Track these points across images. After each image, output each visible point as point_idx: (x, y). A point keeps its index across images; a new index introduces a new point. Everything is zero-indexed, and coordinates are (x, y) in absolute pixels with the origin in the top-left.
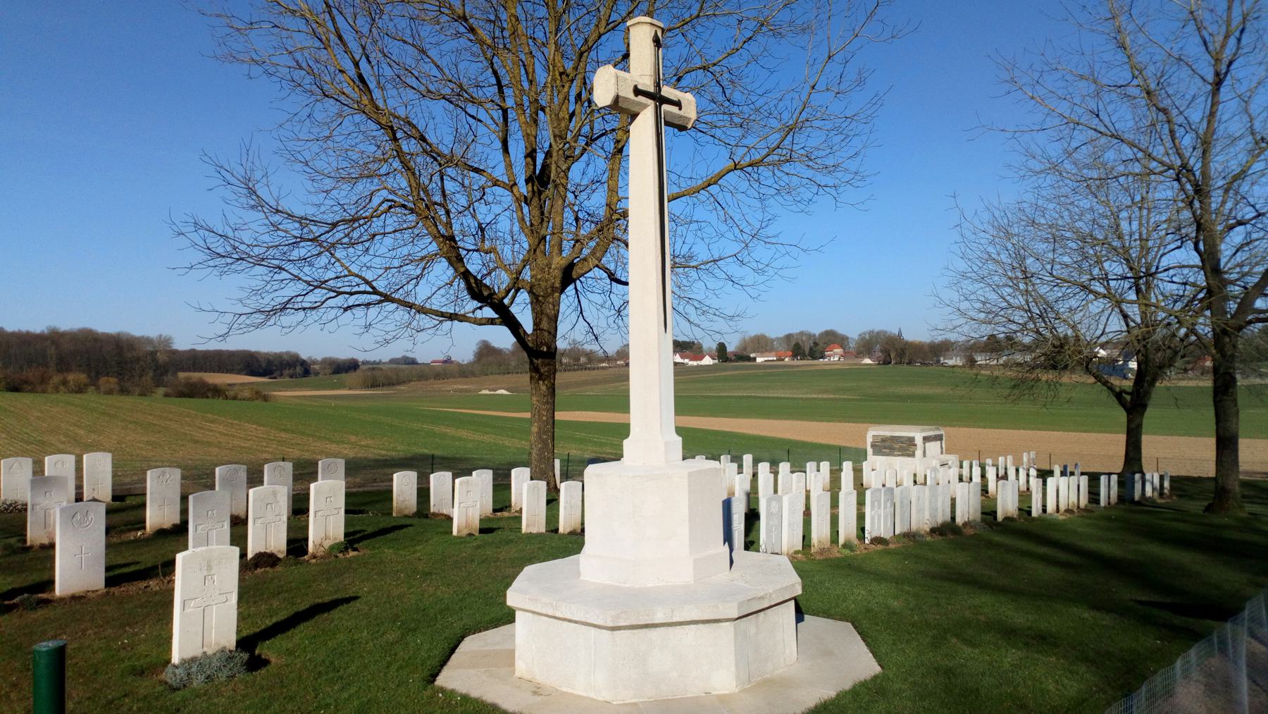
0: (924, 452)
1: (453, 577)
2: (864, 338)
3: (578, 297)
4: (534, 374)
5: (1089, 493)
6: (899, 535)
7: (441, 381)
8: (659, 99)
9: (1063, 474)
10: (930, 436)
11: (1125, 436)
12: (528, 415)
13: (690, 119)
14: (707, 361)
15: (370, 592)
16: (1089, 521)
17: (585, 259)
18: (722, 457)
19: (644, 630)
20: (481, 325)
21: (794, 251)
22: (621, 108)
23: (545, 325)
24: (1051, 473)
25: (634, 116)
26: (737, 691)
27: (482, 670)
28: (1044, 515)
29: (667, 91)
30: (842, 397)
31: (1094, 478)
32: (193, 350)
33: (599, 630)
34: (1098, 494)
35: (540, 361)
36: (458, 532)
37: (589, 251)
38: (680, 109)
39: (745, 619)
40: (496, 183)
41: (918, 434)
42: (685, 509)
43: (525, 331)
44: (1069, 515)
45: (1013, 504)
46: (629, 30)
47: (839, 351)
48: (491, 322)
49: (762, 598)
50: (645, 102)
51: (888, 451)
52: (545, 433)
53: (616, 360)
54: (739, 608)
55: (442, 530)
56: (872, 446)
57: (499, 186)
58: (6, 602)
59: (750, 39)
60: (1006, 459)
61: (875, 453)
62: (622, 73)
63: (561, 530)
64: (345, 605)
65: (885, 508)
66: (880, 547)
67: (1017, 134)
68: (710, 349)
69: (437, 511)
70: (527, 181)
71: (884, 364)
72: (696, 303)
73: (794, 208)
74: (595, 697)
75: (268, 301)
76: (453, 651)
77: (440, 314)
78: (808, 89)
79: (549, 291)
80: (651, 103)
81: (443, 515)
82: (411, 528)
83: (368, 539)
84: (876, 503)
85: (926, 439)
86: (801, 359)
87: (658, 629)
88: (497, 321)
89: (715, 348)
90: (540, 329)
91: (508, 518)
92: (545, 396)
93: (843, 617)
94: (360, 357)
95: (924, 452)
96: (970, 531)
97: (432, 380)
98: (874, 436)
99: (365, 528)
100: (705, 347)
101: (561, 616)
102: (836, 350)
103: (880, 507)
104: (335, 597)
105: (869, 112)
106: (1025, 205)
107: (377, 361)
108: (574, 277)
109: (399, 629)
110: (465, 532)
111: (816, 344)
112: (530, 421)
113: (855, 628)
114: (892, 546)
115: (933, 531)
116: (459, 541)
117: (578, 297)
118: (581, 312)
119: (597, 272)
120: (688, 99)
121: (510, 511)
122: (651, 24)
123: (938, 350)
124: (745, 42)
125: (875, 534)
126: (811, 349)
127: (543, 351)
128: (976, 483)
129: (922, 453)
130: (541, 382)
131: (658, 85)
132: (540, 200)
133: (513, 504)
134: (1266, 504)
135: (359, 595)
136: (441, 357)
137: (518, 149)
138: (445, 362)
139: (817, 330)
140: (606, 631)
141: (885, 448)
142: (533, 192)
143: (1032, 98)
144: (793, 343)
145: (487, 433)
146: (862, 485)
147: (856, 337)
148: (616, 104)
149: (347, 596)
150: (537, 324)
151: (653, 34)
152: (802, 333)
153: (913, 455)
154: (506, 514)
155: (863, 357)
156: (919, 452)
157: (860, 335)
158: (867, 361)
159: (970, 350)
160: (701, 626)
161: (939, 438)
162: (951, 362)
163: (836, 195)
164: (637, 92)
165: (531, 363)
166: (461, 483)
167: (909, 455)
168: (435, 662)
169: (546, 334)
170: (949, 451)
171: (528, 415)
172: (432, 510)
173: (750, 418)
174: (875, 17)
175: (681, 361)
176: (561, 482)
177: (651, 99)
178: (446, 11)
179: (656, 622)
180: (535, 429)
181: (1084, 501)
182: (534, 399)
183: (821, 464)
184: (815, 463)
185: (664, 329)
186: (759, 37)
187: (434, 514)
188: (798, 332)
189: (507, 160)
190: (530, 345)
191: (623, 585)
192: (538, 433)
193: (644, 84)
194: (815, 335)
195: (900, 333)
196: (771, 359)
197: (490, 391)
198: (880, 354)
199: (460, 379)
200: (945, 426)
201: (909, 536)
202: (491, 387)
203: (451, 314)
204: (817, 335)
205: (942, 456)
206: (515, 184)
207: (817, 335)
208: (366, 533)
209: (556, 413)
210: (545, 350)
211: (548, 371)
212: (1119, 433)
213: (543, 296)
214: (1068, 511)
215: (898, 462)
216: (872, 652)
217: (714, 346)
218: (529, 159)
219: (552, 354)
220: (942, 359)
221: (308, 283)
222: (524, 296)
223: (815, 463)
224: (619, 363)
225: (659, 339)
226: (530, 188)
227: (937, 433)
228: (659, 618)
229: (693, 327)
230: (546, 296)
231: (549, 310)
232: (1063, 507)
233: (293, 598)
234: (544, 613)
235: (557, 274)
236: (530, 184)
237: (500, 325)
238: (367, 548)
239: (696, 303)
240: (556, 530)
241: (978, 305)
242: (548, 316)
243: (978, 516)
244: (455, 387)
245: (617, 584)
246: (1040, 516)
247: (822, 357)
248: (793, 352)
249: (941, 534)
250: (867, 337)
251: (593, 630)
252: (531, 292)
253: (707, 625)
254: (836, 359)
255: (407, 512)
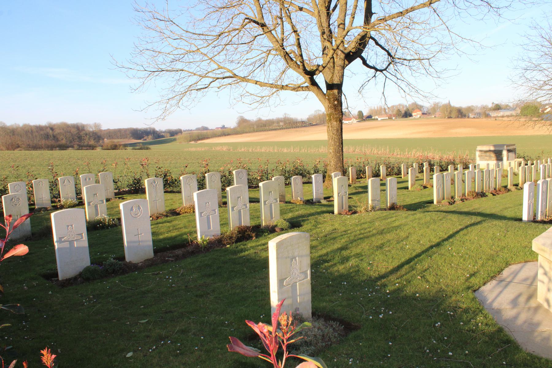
32: (109, 129)
51: (488, 158)
58: (2, 252)
75: (180, 89)
89: (357, 114)
94: (183, 128)
107: (190, 129)
136: (220, 126)
152: (400, 105)
176: (334, 178)
196: (386, 118)
221: (200, 76)
233: (221, 256)
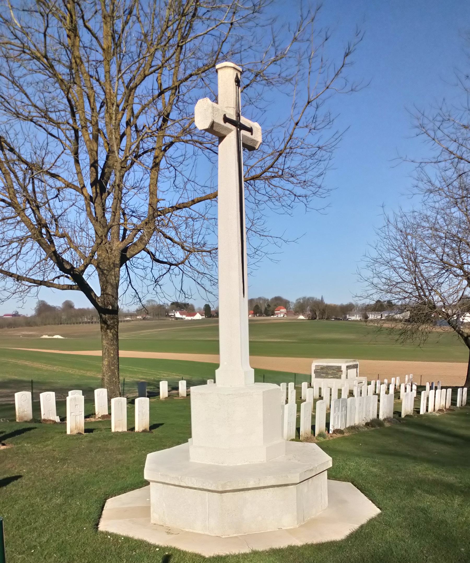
0: (347, 376)
1: (82, 461)
2: (300, 302)
3: (128, 271)
4: (103, 325)
5: (452, 400)
6: (349, 427)
7: (13, 329)
8: (240, 127)
9: (431, 388)
10: (350, 366)
11: (468, 364)
12: (99, 353)
13: (257, 142)
14: (198, 317)
15: (28, 473)
16: (455, 417)
17: (135, 244)
18: (208, 381)
19: (241, 492)
20: (63, 289)
21: (279, 242)
22: (215, 131)
23: (109, 291)
24: (424, 388)
25: (221, 138)
26: (297, 526)
27: (128, 520)
28: (427, 413)
29: (244, 120)
30: (286, 341)
31: (455, 390)
33: (211, 493)
34: (456, 401)
35: (107, 316)
36: (71, 432)
37: (137, 239)
38: (252, 134)
39: (302, 483)
40: (68, 185)
41: (343, 364)
42: (260, 415)
43: (95, 295)
44: (441, 413)
45: (411, 407)
46: (217, 71)
47: (284, 310)
48: (70, 287)
49: (311, 470)
50: (230, 128)
52: (113, 365)
53: (136, 316)
54: (300, 477)
55: (58, 431)
56: (315, 372)
57: (71, 188)
59: (248, 86)
60: (396, 379)
61: (316, 377)
62: (215, 104)
63: (137, 429)
64: (15, 481)
65: (342, 411)
66: (339, 435)
67: (423, 164)
68: (199, 309)
69: (46, 418)
70: (92, 185)
71: (312, 319)
72: (209, 276)
73: (282, 210)
74: (209, 534)
76: (103, 507)
77: (33, 281)
78: (293, 125)
79: (112, 266)
80: (233, 128)
81: (51, 420)
82: (37, 429)
83: (10, 437)
84: (337, 408)
85: (348, 367)
86: (259, 316)
87: (250, 491)
88: (74, 287)
90: (106, 294)
91: (95, 422)
92: (112, 340)
93: (345, 479)
95: (347, 376)
96: (387, 425)
97: (6, 328)
98: (316, 366)
99: (4, 430)
100: (196, 307)
101: (185, 485)
102: (282, 310)
103: (339, 411)
104: (6, 476)
105: (333, 144)
106: (416, 214)
108: (128, 257)
109: (61, 495)
110: (75, 432)
111: (269, 306)
112: (102, 358)
113: (355, 486)
114: (346, 434)
115: (367, 424)
116: (75, 438)
117: (128, 271)
118: (130, 282)
119: (144, 253)
120: (256, 126)
121: (95, 417)
122: (234, 68)
123: (348, 309)
124: (245, 88)
125: (336, 428)
126: (266, 309)
127: (109, 309)
128: (391, 395)
129: (345, 376)
130: (108, 331)
131: (238, 116)
132: (102, 199)
133: (97, 414)
134: (2, 405)
135: (23, 474)
136: (11, 312)
137: (85, 158)
138: (13, 315)
139: (270, 296)
140: (216, 494)
141: (323, 373)
142: (97, 193)
143: (434, 139)
144: (254, 305)
145: (56, 365)
146: (301, 398)
147: (295, 302)
148: (212, 129)
149: (13, 475)
150: (103, 290)
151: (235, 76)
152: (260, 298)
153: (340, 377)
154: (92, 419)
155: (299, 315)
156: (343, 376)
157: (297, 300)
158: (301, 317)
159: (366, 309)
160: (276, 488)
161: (355, 366)
162: (353, 318)
163: (306, 203)
164: (226, 120)
165: (101, 317)
166: (116, 402)
167: (337, 378)
168: (96, 516)
169: (111, 297)
170: (361, 374)
171: (99, 353)
172: (43, 417)
173: (177, 353)
174: (340, 75)
175: (180, 316)
177: (234, 125)
178: (27, 51)
179: (250, 487)
180: (106, 363)
181: (448, 405)
182: (105, 342)
183: (289, 384)
184: (286, 384)
185: (243, 295)
186: (254, 85)
187: (44, 420)
188: (257, 297)
189: (78, 168)
190: (100, 305)
191: (221, 465)
192: (108, 365)
193: (230, 114)
194: (268, 300)
195: (322, 298)
197: (49, 336)
198: (310, 313)
199: (26, 328)
200: (359, 359)
201: (353, 428)
202: (49, 333)
203: (41, 281)
204: (270, 299)
205: (357, 378)
206: (84, 186)
207: (270, 299)
208: (7, 433)
209: (119, 351)
210: (111, 308)
211: (114, 323)
212: (463, 362)
213: (107, 270)
214: (440, 410)
215: (334, 383)
216: (370, 500)
217: (202, 307)
218: (93, 168)
219: (115, 311)
220: (348, 316)
222: (91, 269)
223: (286, 384)
224: (138, 317)
225: (240, 302)
226: (94, 190)
227: (354, 363)
228: (251, 485)
229: (208, 293)
230: (109, 270)
231: (112, 280)
232: (437, 408)
234: (173, 483)
235: (117, 253)
236: (94, 187)
237: (77, 289)
238: (11, 443)
239: (209, 276)
240: (133, 429)
241: (384, 280)
242: (111, 284)
243: (391, 415)
244: (23, 333)
245: (217, 464)
246: (425, 414)
247: (273, 315)
248: (254, 311)
249: (372, 426)
250: (302, 301)
251: (207, 493)
252: (98, 267)
253: (280, 488)
254: (282, 316)
255: (26, 419)
